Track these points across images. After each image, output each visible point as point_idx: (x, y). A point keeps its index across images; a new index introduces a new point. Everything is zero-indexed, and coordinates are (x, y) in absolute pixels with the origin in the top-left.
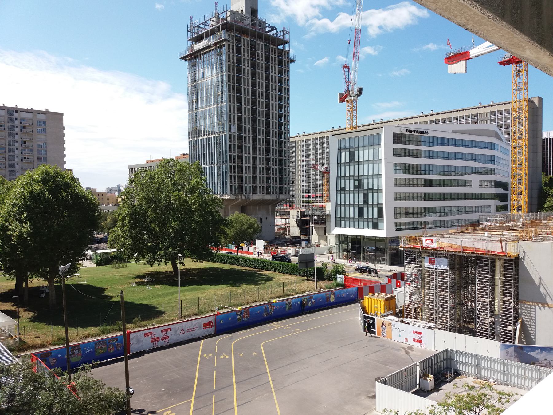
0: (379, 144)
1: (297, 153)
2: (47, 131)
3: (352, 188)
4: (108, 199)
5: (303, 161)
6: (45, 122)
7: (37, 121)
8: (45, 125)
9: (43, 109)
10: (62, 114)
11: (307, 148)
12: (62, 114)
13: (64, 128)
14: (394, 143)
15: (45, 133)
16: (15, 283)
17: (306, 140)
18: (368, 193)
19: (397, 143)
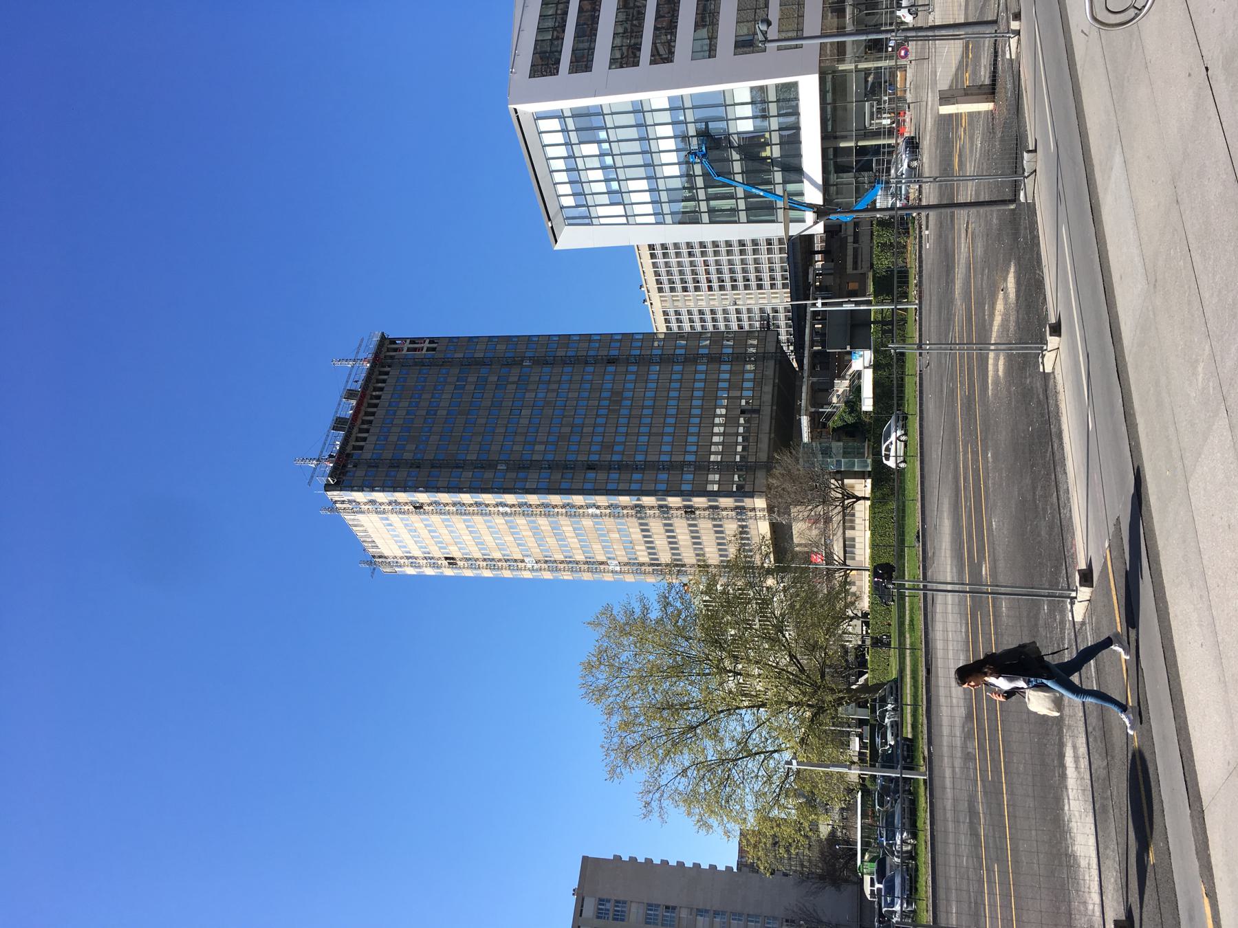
0: (599, 112)
1: (692, 304)
2: (622, 898)
3: (619, 210)
4: (1190, 75)
5: (710, 288)
6: (600, 900)
7: (598, 917)
8: (608, 901)
9: (573, 900)
10: (585, 859)
11: (677, 278)
12: (585, 859)
13: (618, 858)
14: (636, 64)
15: (625, 902)
16: (1075, 682)
17: (659, 282)
18: (738, 133)
19: (558, 62)
